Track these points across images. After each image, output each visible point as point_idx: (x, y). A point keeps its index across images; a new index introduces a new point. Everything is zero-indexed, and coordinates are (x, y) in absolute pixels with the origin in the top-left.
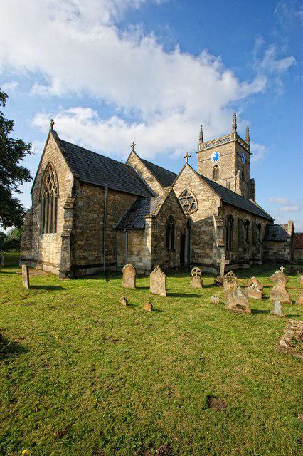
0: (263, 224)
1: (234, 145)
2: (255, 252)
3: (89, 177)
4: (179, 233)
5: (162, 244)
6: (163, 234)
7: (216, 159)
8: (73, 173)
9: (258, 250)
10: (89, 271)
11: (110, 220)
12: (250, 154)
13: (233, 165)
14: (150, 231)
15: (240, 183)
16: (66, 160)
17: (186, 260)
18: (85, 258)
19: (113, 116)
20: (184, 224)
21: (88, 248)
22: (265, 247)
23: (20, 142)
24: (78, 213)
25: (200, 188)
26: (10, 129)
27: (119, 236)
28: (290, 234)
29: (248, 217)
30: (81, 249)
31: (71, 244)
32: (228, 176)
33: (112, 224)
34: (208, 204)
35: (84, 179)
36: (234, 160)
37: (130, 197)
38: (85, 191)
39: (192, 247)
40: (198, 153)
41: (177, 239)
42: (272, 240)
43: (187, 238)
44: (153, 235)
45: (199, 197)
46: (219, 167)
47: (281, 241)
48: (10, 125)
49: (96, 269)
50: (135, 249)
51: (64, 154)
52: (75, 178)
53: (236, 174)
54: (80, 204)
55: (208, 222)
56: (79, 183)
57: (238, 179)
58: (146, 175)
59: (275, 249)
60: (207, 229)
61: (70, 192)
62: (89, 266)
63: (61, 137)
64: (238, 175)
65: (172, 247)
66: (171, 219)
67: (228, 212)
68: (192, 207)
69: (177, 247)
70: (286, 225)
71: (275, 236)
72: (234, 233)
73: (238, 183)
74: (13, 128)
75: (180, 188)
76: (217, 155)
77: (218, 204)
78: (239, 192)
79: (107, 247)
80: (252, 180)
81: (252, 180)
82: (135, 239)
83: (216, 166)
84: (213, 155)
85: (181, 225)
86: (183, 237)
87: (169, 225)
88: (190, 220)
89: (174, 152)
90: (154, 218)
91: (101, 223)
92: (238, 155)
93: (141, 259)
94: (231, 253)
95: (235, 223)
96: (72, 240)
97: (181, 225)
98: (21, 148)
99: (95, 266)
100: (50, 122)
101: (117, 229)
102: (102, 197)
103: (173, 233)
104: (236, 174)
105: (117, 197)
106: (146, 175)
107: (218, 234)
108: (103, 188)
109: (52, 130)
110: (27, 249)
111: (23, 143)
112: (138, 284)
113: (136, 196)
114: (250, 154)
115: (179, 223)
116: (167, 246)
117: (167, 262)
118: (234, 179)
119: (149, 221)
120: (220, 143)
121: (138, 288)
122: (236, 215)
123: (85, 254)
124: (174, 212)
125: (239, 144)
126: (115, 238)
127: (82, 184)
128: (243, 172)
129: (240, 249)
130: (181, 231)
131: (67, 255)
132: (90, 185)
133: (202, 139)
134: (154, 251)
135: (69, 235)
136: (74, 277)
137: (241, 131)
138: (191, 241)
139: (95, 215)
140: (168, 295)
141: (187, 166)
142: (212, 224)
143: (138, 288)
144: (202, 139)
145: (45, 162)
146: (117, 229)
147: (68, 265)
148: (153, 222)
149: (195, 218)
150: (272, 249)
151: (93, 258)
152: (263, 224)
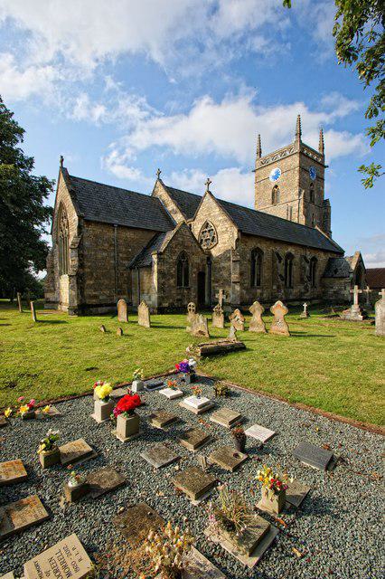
0: (322, 258)
1: (297, 158)
2: (303, 290)
3: (97, 214)
4: (195, 270)
5: (172, 281)
6: (173, 270)
7: (276, 177)
8: (77, 212)
9: (306, 287)
10: (100, 310)
11: (122, 259)
12: (325, 167)
13: (296, 182)
14: (155, 267)
15: (305, 207)
16: (72, 199)
17: (206, 299)
18: (95, 297)
19: (299, 101)
20: (202, 260)
21: (97, 287)
22: (323, 286)
23: (44, 179)
24: (86, 253)
25: (220, 218)
26: (31, 167)
27: (134, 274)
28: (353, 267)
29: (291, 250)
30: (91, 288)
31: (77, 283)
32: (289, 198)
33: (125, 262)
34: (226, 236)
35: (91, 217)
36: (297, 178)
37: (146, 233)
38: (91, 230)
39: (213, 285)
40: (255, 171)
41: (193, 276)
42: (332, 277)
43: (207, 276)
44: (159, 272)
45: (219, 229)
46: (279, 187)
47: (343, 278)
48: (30, 162)
49: (109, 308)
50: (146, 286)
51: (71, 192)
52: (80, 217)
53: (299, 196)
54: (87, 243)
55: (225, 257)
56: (84, 222)
57: (302, 201)
58: (171, 206)
59: (336, 288)
60: (225, 265)
61: (76, 231)
62: (101, 305)
63: (71, 173)
64: (302, 196)
65: (186, 284)
66: (183, 255)
67: (252, 244)
68: (212, 241)
69: (193, 286)
70: (352, 257)
71: (336, 271)
72: (264, 268)
73: (302, 206)
74: (34, 165)
75: (201, 220)
76: (277, 173)
77: (236, 236)
78: (303, 222)
79: (120, 287)
80: (327, 201)
81: (327, 201)
82: (146, 278)
83: (276, 187)
84: (273, 173)
85: (199, 261)
86: (201, 275)
87: (180, 261)
88: (210, 256)
89: (241, 173)
90: (159, 254)
91: (112, 262)
92: (303, 169)
93: (150, 297)
94: (259, 291)
95: (266, 258)
96: (79, 280)
97: (199, 261)
98: (44, 186)
99: (107, 305)
100: (60, 159)
101: (131, 268)
102: (112, 234)
103: (187, 270)
104: (299, 196)
105: (130, 235)
106: (171, 206)
107: (234, 269)
108: (112, 225)
109: (62, 167)
110: (51, 291)
111: (47, 181)
112: (39, 318)
113: (155, 231)
114: (325, 167)
115: (196, 259)
116: (179, 283)
117: (178, 300)
118: (297, 202)
119: (155, 258)
120: (284, 155)
121: (293, 334)
122: (267, 249)
123: (96, 293)
124: (187, 247)
125: (307, 156)
126: (129, 278)
127: (88, 222)
128: (312, 192)
129: (275, 287)
130: (198, 269)
131: (74, 293)
132: (97, 223)
133: (260, 152)
134: (161, 287)
135: (74, 274)
136: (83, 314)
137: (312, 141)
138: (212, 279)
139: (105, 254)
140: (151, 327)
141: (208, 195)
142: (229, 259)
143: (293, 334)
144: (260, 152)
145: (58, 202)
146: (131, 268)
147: (76, 304)
148: (159, 259)
149: (215, 252)
150: (332, 288)
151: (105, 297)
152: (322, 258)
